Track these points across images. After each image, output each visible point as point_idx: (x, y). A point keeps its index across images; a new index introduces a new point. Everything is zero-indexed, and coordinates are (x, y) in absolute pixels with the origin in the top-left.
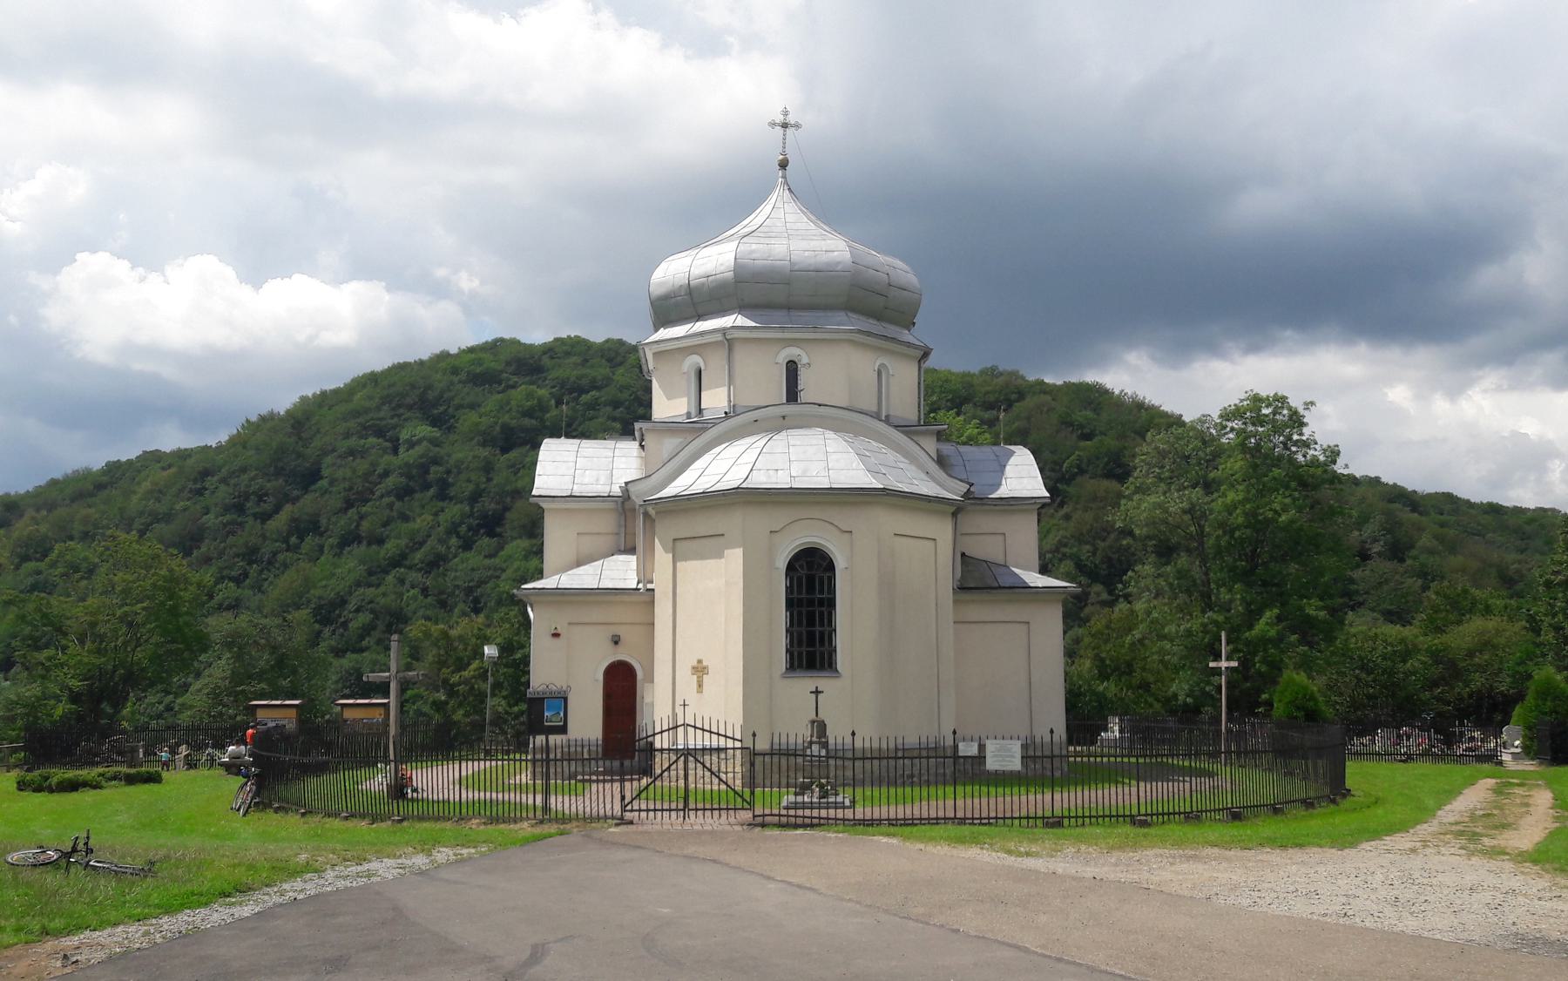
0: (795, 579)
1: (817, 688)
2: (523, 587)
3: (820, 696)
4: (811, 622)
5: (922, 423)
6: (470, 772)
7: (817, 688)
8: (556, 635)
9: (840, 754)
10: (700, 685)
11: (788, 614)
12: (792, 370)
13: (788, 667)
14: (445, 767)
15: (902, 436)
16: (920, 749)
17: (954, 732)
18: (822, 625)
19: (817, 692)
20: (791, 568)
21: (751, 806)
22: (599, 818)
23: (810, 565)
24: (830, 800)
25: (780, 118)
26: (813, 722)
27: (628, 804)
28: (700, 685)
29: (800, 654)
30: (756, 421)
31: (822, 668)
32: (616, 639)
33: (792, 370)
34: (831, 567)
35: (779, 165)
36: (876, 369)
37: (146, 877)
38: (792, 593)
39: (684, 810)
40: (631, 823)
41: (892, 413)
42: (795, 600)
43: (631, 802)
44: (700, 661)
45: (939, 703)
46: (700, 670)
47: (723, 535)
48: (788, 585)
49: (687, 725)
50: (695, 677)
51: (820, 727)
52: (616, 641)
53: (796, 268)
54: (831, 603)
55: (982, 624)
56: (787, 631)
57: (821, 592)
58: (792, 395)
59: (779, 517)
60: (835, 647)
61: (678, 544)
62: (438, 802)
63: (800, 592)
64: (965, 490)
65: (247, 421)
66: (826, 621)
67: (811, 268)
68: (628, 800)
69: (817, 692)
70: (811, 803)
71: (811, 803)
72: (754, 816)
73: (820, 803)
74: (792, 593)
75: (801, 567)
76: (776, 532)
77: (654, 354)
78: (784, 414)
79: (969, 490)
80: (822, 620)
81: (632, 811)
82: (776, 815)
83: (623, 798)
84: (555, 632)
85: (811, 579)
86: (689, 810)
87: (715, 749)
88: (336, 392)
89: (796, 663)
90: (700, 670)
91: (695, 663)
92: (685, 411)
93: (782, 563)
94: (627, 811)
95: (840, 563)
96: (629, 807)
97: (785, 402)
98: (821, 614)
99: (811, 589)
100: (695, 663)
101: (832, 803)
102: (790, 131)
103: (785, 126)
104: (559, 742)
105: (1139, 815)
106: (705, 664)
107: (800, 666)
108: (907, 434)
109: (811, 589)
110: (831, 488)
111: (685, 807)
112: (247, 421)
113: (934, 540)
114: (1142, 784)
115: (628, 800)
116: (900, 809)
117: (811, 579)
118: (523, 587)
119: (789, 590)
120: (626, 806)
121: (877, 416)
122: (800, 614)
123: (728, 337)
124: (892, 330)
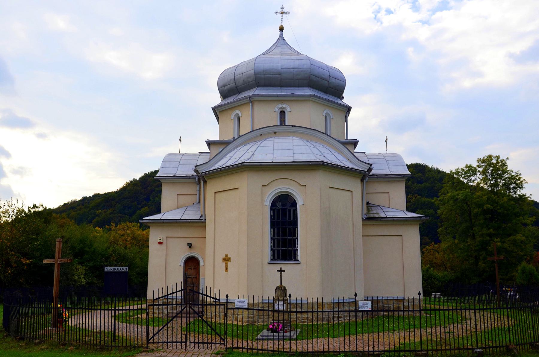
1: (281, 268)
2: (144, 218)
3: (283, 273)
8: (160, 243)
10: (227, 268)
11: (272, 229)
12: (282, 113)
13: (272, 258)
14: (87, 313)
15: (341, 145)
16: (268, 303)
18: (290, 235)
19: (281, 271)
20: (273, 206)
21: (225, 344)
22: (138, 347)
24: (280, 335)
25: (280, 10)
26: (278, 288)
27: (151, 338)
28: (227, 268)
29: (278, 251)
30: (261, 135)
31: (290, 259)
32: (190, 245)
33: (282, 113)
35: (280, 30)
36: (324, 115)
37: (111, 350)
38: (274, 218)
39: (186, 342)
43: (153, 337)
44: (227, 256)
45: (355, 277)
46: (226, 260)
48: (272, 214)
51: (281, 290)
52: (190, 246)
53: (284, 67)
54: (295, 224)
56: (271, 239)
57: (290, 218)
59: (266, 178)
60: (297, 247)
61: (217, 194)
62: (97, 333)
63: (278, 218)
64: (368, 168)
67: (291, 67)
68: (151, 336)
69: (281, 271)
70: (268, 336)
71: (268, 336)
72: (226, 348)
74: (274, 218)
76: (266, 186)
77: (219, 112)
78: (274, 131)
79: (370, 168)
81: (154, 343)
82: (241, 348)
83: (148, 334)
86: (190, 343)
90: (226, 260)
91: (224, 257)
92: (233, 137)
94: (151, 343)
95: (299, 203)
96: (151, 341)
98: (290, 229)
100: (224, 257)
101: (281, 336)
102: (284, 15)
103: (282, 13)
104: (245, 302)
105: (478, 348)
106: (229, 257)
107: (278, 258)
110: (294, 162)
111: (186, 340)
113: (352, 191)
115: (151, 336)
118: (144, 218)
119: (272, 217)
121: (326, 134)
122: (278, 230)
123: (251, 100)
124: (331, 98)
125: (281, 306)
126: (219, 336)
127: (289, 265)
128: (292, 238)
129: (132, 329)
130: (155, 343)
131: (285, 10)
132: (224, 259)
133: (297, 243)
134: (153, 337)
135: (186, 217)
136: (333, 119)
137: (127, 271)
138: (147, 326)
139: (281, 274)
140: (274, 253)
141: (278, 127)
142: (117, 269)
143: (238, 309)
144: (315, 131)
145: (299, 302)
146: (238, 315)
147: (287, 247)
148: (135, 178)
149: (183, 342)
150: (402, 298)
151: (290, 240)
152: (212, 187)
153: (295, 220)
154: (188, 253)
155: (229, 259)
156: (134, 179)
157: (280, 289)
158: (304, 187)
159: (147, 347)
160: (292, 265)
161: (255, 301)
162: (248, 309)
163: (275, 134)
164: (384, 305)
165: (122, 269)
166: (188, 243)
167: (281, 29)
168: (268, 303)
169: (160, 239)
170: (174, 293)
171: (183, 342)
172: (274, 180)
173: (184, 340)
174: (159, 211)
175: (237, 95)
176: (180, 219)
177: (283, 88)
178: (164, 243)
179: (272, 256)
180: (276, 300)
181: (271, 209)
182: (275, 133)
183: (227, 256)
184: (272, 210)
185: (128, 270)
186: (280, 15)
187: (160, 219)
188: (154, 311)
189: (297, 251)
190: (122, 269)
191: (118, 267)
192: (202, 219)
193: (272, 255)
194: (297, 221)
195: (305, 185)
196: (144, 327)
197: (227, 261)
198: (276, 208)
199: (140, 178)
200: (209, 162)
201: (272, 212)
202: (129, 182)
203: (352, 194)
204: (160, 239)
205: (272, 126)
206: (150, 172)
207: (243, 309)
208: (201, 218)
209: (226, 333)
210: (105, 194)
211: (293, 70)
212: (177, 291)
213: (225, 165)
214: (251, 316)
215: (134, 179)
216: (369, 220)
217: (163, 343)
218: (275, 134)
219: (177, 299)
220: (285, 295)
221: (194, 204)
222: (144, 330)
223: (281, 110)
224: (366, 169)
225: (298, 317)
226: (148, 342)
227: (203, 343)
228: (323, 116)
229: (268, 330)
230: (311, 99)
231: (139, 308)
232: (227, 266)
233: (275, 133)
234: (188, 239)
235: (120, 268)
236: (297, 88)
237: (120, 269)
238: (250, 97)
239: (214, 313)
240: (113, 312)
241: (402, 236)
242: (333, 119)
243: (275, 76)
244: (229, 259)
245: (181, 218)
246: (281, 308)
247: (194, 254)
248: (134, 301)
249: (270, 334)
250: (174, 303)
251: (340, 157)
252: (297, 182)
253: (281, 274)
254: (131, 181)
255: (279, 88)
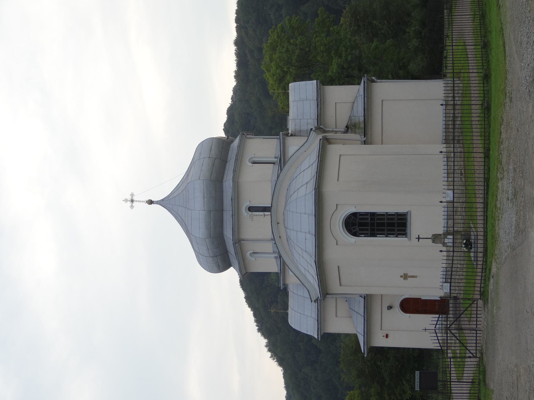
0: (360, 232)
1: (416, 238)
2: (363, 352)
3: (420, 237)
4: (383, 224)
5: (279, 137)
6: (455, 378)
7: (416, 238)
8: (387, 336)
9: (451, 262)
10: (413, 277)
11: (378, 236)
12: (251, 209)
13: (405, 236)
15: (285, 167)
16: (445, 278)
17: (441, 202)
18: (384, 219)
19: (419, 238)
20: (355, 234)
21: (477, 300)
23: (354, 224)
25: (129, 204)
26: (434, 242)
27: (473, 355)
28: (413, 277)
29: (399, 230)
30: (280, 237)
31: (406, 219)
32: (389, 308)
34: (354, 214)
36: (251, 165)
38: (367, 234)
39: (476, 331)
40: (482, 354)
41: (273, 156)
42: (371, 232)
43: (472, 354)
44: (401, 277)
46: (405, 277)
47: (338, 181)
48: (364, 236)
49: (435, 328)
50: (409, 279)
51: (436, 238)
52: (390, 308)
54: (373, 214)
55: (383, 125)
56: (387, 237)
57: (367, 219)
58: (265, 209)
60: (395, 213)
61: (343, 284)
63: (367, 230)
65: (271, 357)
66: (382, 217)
67: (203, 200)
68: (471, 355)
73: (474, 247)
74: (367, 234)
75: (354, 229)
76: (337, 241)
80: (381, 219)
81: (476, 353)
84: (385, 336)
85: (361, 224)
86: (477, 328)
87: (454, 126)
88: (255, 315)
89: (404, 232)
90: (405, 277)
93: (353, 239)
95: (353, 210)
96: (475, 355)
97: (269, 213)
98: (378, 219)
99: (366, 224)
100: (402, 278)
102: (135, 198)
103: (132, 201)
106: (402, 274)
107: (405, 230)
108: (284, 164)
109: (366, 224)
111: (475, 330)
112: (271, 357)
114: (453, 392)
115: (471, 355)
116: (479, 214)
117: (361, 224)
119: (366, 235)
120: (475, 356)
122: (378, 230)
125: (449, 240)
126: (471, 304)
127: (412, 221)
128: (386, 217)
129: (469, 363)
130: (476, 352)
131: (129, 198)
132: (405, 279)
133: (391, 213)
134: (472, 354)
135: (361, 311)
136: (254, 154)
137: (419, 372)
138: (465, 357)
139: (421, 238)
140: (400, 234)
141: (278, 245)
142: (417, 380)
143: (450, 290)
144: (276, 185)
145: (446, 217)
146: (457, 268)
147: (395, 222)
148: (265, 344)
149: (476, 332)
150: (445, 101)
151: (388, 219)
152: (334, 287)
153: (369, 214)
154: (397, 309)
155: (405, 274)
156: (266, 346)
157: (434, 240)
158: (338, 206)
159: (479, 358)
160: (412, 219)
161: (445, 258)
162: (450, 283)
163: (279, 223)
164: (451, 120)
165: (417, 376)
166: (388, 310)
167: (151, 202)
168: (445, 278)
169: (384, 336)
170: (439, 341)
171: (476, 332)
172: (332, 233)
173: (475, 332)
174: (355, 336)
175: (229, 253)
176: (364, 317)
177: (225, 209)
178: (386, 332)
179: (403, 236)
180: (444, 244)
181: (358, 236)
182: (278, 223)
183: (401, 277)
184: (360, 235)
185: (418, 371)
186: (135, 204)
187: (364, 336)
188: (453, 342)
189: (399, 213)
190: (417, 376)
191: (416, 379)
192: (364, 296)
193: (401, 236)
194: (370, 212)
195: (337, 205)
196: (467, 360)
197: (406, 276)
198: (358, 232)
199: (265, 338)
200: (308, 288)
201: (361, 236)
202: (269, 354)
203: (343, 155)
204: (384, 336)
205: (272, 227)
206: (256, 323)
207: (450, 286)
208: (363, 297)
209: (469, 299)
210: (287, 387)
211: (206, 199)
212: (436, 336)
213: (314, 276)
214: (458, 258)
215: (266, 346)
216: (367, 134)
217: (476, 347)
218: (279, 223)
219: (442, 321)
220: (440, 236)
221: (346, 301)
222: (469, 360)
223: (248, 211)
224: (315, 134)
225: (460, 214)
226: (476, 357)
227: (477, 317)
228: (252, 166)
229: (470, 252)
230: (236, 180)
231: (452, 242)
232: (411, 276)
233: (278, 223)
234: (383, 309)
235: (416, 378)
236: (225, 194)
237: (418, 378)
238: (234, 244)
239: (455, 280)
240: (451, 44)
241: (382, 100)
242: (254, 154)
243: (212, 216)
244: (405, 274)
245: (363, 316)
246: (451, 241)
247: (397, 304)
248: (447, 385)
249: (473, 250)
250: (446, 323)
251: (306, 164)
252: (334, 212)
253: (421, 238)
254: (269, 350)
255: (225, 213)
